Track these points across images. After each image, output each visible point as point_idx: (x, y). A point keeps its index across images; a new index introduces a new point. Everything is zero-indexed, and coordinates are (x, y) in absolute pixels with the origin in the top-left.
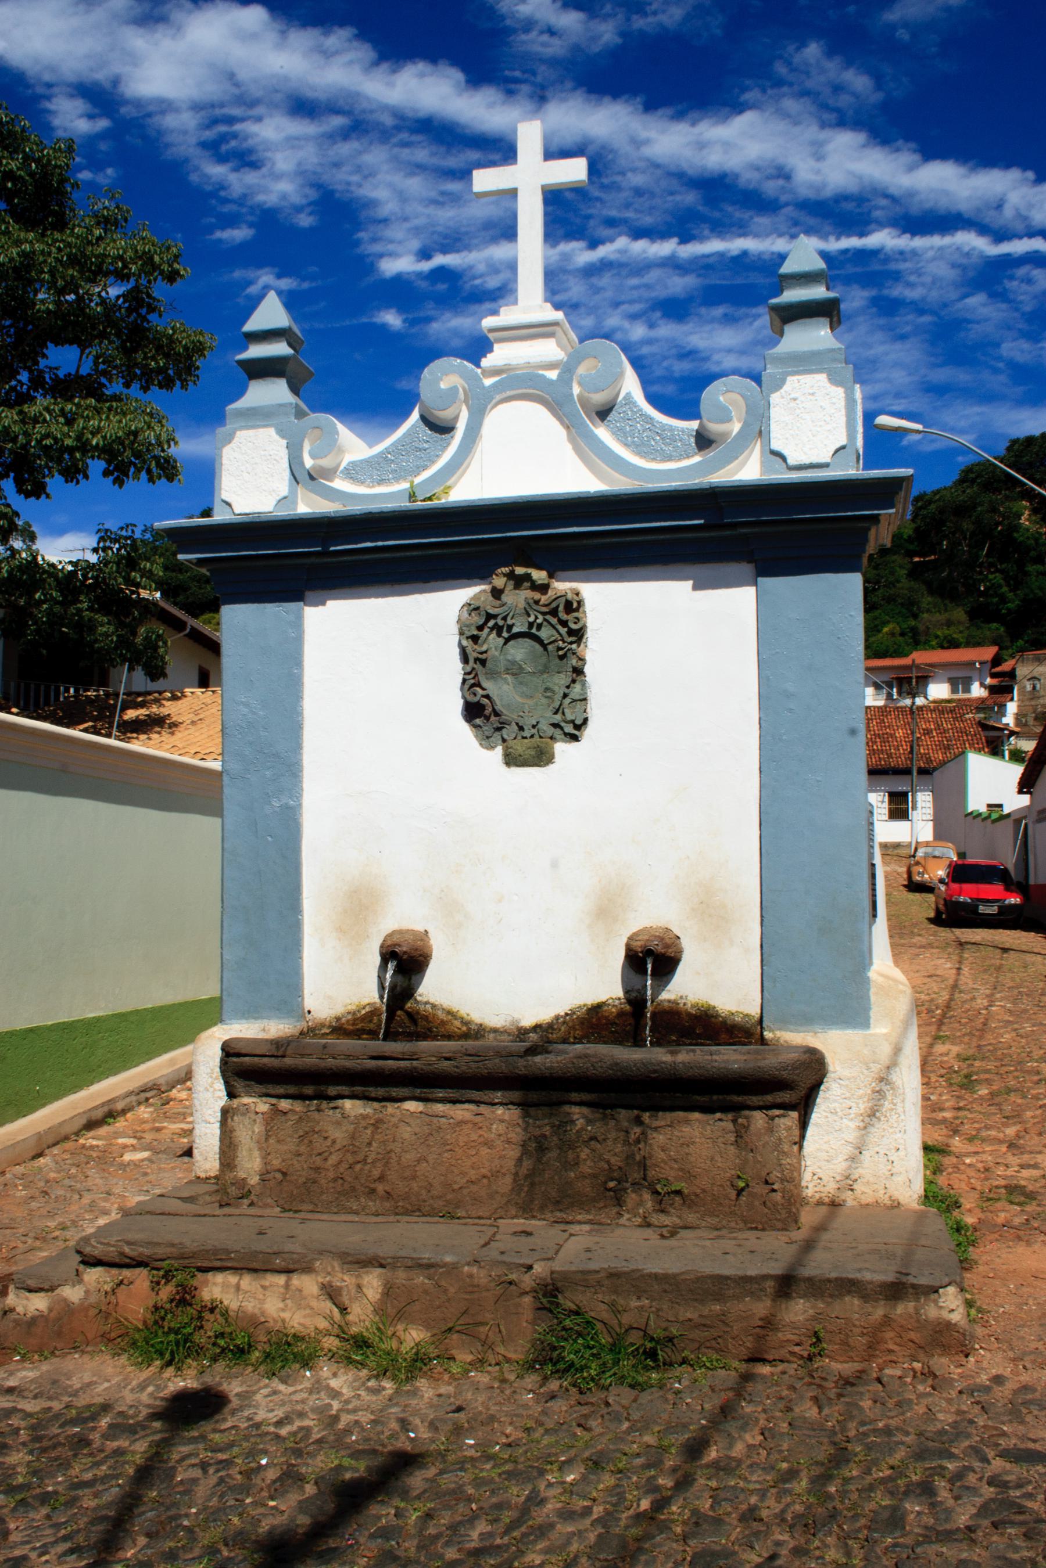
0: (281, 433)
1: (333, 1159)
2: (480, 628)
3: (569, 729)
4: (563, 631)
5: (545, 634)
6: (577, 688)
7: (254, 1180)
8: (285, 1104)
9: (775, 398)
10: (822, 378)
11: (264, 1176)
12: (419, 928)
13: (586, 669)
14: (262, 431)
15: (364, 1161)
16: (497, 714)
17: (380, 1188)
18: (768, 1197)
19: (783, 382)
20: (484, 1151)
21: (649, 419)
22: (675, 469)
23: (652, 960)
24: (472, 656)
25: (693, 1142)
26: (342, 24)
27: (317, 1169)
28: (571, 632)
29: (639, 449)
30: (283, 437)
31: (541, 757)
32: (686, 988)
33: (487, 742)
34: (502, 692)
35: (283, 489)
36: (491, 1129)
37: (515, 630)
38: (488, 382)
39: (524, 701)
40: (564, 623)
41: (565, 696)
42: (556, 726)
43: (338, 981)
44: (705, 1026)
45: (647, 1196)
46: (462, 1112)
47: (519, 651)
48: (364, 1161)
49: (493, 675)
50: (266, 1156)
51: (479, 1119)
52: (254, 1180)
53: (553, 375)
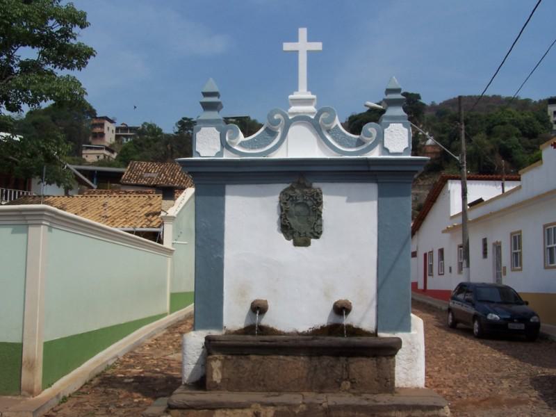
0: (218, 129)
1: (247, 374)
2: (287, 200)
3: (316, 235)
4: (315, 202)
5: (309, 203)
6: (319, 221)
7: (219, 381)
8: (229, 357)
9: (386, 130)
10: (401, 125)
11: (223, 380)
12: (264, 299)
13: (323, 215)
14: (210, 128)
15: (257, 375)
16: (291, 229)
17: (262, 383)
18: (386, 383)
19: (389, 125)
20: (297, 371)
21: (344, 134)
22: (350, 153)
23: (341, 309)
24: (284, 210)
25: (364, 367)
26: (298, 30)
27: (241, 378)
28: (318, 203)
29: (340, 143)
30: (218, 131)
31: (306, 243)
32: (352, 319)
33: (288, 238)
34: (294, 222)
35: (218, 149)
36: (298, 365)
37: (299, 201)
38: (290, 118)
39: (301, 224)
40: (316, 200)
41: (315, 223)
42: (311, 233)
43: (234, 317)
44: (355, 332)
45: (349, 383)
46: (289, 359)
47: (299, 209)
48: (257, 375)
49: (291, 216)
50: (223, 373)
51: (295, 361)
52: (219, 381)
53: (313, 117)
